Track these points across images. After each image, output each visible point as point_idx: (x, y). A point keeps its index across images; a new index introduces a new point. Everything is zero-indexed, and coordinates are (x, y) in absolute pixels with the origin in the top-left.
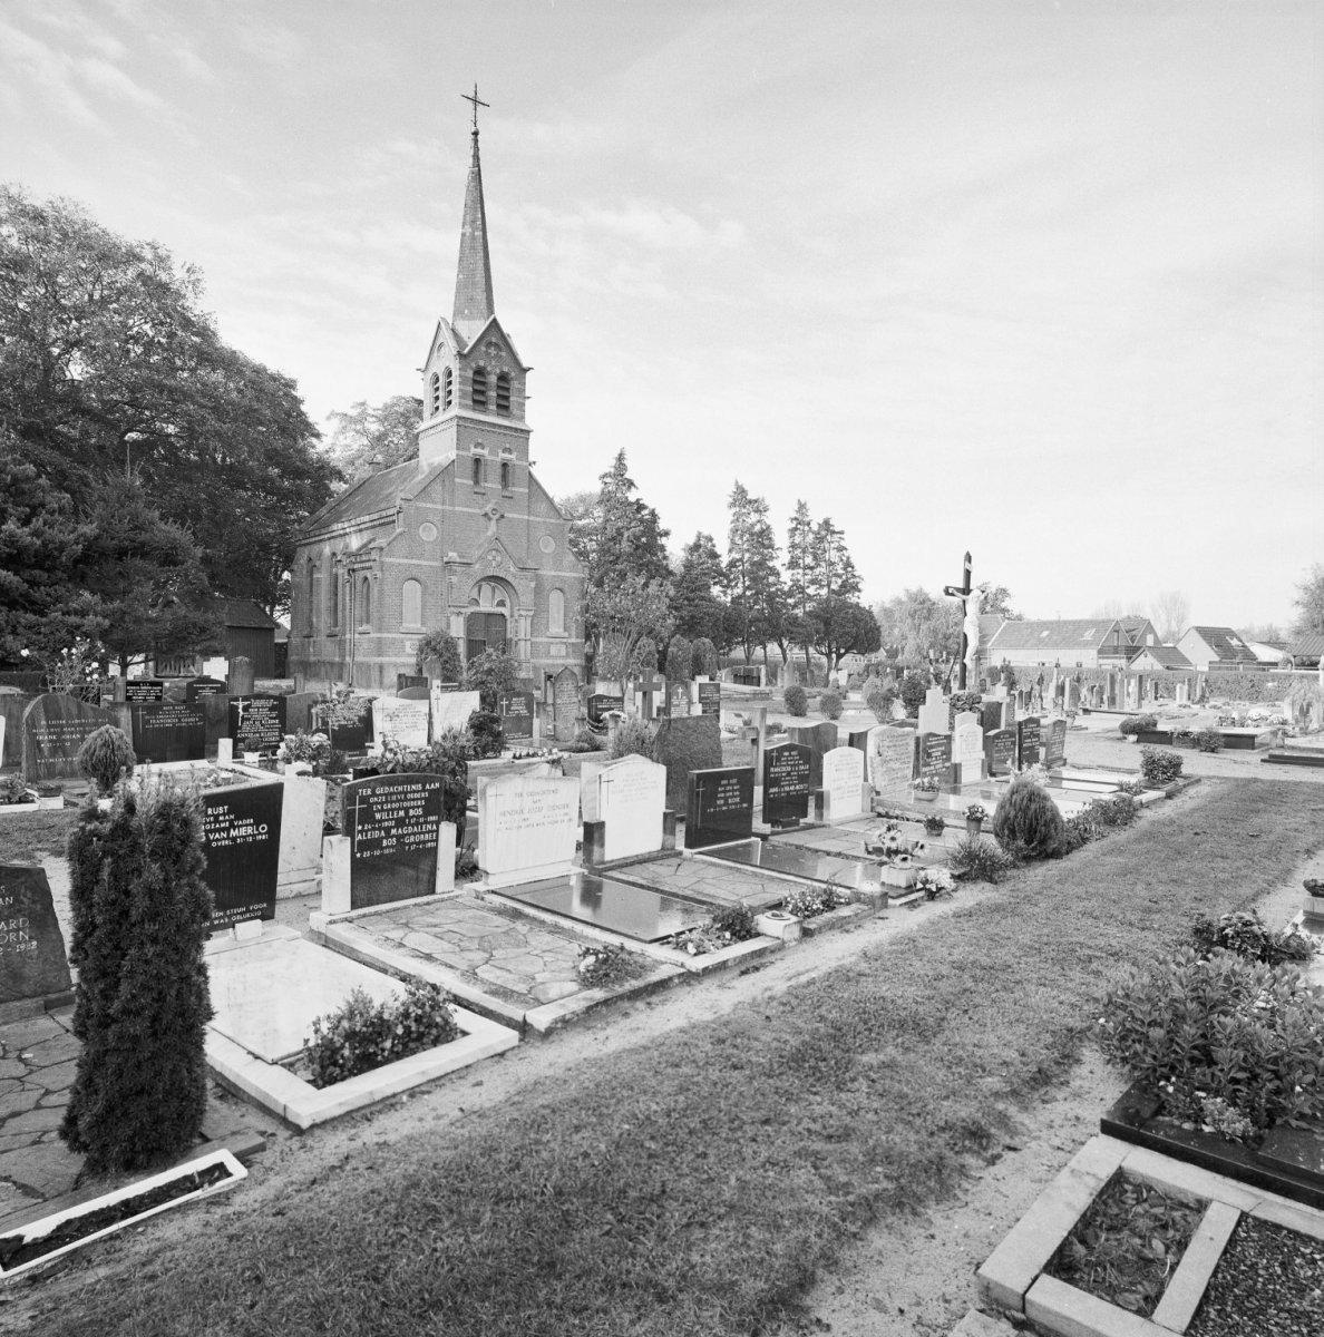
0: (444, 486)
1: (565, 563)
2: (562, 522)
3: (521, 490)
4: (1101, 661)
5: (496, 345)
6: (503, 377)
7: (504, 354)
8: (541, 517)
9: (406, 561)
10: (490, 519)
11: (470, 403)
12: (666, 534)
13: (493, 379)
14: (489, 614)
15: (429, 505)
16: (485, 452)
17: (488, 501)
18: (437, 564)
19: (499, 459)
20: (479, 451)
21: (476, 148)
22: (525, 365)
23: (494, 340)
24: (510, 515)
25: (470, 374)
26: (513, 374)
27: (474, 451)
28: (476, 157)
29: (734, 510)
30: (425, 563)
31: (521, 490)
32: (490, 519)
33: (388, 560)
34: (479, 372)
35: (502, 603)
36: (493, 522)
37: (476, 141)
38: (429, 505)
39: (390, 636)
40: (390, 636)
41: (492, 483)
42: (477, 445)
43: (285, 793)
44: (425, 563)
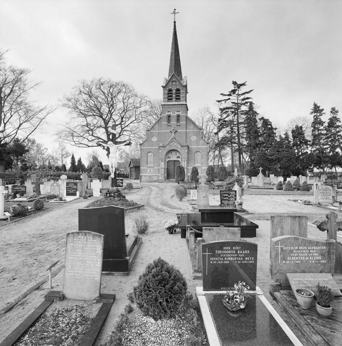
0: (159, 125)
1: (200, 143)
2: (199, 130)
3: (183, 122)
4: (241, 238)
5: (175, 81)
6: (178, 90)
7: (177, 83)
8: (191, 129)
9: (148, 147)
10: (172, 133)
11: (167, 100)
12: (276, 129)
13: (174, 91)
14: (175, 161)
15: (155, 131)
16: (171, 113)
17: (172, 128)
18: (158, 147)
19: (175, 115)
20: (178, 113)
21: (175, 26)
22: (188, 92)
23: (174, 80)
24: (179, 131)
25: (167, 92)
26: (180, 88)
27: (176, 113)
28: (175, 29)
29: (313, 115)
30: (154, 147)
31: (183, 122)
32: (172, 133)
33: (143, 148)
34: (170, 90)
35: (178, 157)
36: (173, 134)
37: (175, 24)
38: (155, 131)
39: (143, 168)
40: (143, 168)
41: (173, 122)
42: (177, 111)
43: (80, 209)
44: (154, 147)
